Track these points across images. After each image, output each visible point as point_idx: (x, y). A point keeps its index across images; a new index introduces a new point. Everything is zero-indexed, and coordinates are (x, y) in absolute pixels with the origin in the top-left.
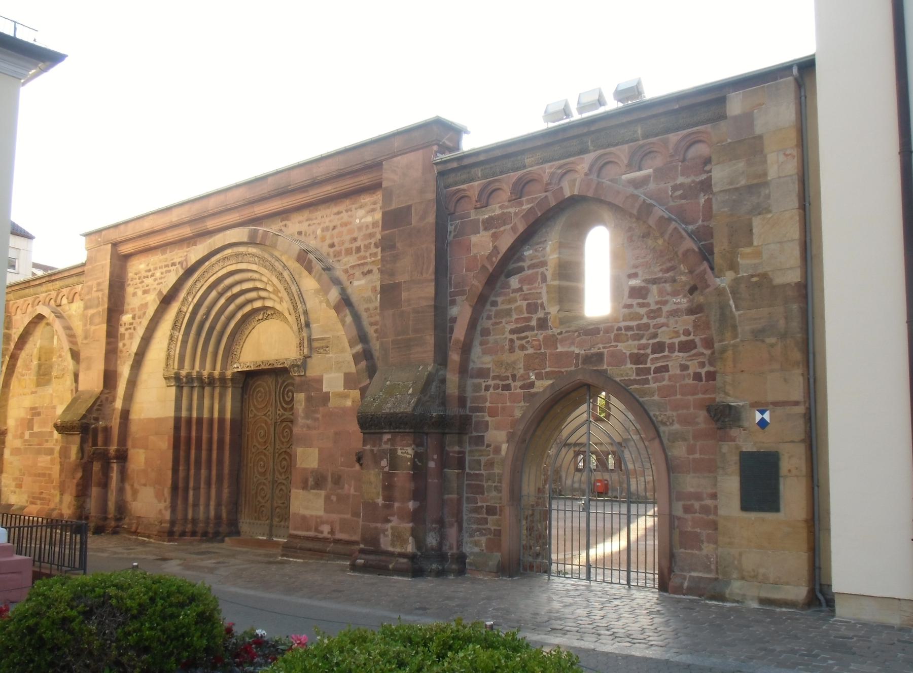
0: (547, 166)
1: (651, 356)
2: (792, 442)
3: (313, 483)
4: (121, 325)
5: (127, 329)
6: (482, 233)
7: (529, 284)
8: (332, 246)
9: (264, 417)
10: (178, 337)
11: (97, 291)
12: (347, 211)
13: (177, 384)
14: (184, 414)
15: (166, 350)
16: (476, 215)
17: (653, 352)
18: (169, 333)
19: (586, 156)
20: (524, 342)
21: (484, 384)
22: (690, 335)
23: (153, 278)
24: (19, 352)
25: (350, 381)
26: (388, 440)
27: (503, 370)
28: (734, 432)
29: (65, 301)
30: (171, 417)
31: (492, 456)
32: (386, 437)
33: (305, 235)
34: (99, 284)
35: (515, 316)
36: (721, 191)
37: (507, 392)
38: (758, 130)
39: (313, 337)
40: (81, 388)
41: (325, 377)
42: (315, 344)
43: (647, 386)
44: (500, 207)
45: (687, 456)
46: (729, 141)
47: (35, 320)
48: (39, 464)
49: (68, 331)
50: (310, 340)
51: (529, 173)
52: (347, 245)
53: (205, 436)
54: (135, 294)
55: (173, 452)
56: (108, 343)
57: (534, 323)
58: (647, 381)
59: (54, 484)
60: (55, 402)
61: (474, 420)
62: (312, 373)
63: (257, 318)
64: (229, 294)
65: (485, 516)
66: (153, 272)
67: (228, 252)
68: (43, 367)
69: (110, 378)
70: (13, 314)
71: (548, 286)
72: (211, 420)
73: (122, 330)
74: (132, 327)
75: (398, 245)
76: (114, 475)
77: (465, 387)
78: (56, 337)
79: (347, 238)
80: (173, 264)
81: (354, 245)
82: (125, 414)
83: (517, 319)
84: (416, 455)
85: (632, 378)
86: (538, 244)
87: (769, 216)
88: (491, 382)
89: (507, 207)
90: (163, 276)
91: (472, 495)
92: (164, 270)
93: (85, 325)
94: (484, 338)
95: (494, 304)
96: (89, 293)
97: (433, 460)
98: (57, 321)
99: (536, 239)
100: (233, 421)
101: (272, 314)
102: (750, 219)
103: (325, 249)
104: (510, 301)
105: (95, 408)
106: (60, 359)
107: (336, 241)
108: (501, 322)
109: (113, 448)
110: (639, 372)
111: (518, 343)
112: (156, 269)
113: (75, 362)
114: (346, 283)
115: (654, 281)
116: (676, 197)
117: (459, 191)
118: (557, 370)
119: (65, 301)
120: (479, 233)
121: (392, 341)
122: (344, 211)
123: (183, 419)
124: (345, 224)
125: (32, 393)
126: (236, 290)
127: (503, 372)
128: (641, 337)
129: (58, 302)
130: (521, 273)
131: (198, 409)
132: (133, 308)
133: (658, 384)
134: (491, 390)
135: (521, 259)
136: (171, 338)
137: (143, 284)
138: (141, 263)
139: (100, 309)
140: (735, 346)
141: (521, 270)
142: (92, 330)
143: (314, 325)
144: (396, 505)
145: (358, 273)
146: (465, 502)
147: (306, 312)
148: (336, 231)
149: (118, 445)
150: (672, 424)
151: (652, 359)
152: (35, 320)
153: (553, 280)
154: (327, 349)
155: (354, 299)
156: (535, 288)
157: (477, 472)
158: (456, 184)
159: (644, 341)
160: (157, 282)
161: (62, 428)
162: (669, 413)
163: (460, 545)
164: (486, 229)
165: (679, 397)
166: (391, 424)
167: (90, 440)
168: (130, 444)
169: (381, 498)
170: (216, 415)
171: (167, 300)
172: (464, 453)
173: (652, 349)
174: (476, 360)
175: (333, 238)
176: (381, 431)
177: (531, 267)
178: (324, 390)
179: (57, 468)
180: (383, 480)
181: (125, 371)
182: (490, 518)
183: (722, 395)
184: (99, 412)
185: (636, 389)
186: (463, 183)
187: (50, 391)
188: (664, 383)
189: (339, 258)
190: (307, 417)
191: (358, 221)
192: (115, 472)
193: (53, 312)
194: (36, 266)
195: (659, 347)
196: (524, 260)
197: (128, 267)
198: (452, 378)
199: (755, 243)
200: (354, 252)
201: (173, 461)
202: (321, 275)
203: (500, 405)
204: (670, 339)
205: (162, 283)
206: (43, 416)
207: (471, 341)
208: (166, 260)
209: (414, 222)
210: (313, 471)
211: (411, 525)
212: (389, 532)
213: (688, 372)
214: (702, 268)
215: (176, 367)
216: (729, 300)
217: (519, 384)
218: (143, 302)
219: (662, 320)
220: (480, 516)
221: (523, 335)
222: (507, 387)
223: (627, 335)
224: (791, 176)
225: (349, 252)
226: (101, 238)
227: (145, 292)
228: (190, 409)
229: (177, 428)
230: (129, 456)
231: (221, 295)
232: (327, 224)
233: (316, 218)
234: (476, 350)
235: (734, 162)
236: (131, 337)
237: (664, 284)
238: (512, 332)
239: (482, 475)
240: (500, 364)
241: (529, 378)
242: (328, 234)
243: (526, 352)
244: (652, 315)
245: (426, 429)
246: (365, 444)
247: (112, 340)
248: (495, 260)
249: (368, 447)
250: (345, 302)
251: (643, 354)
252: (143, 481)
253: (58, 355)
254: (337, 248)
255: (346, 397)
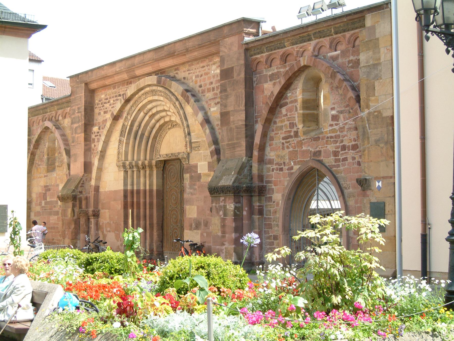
0: (295, 46)
1: (341, 152)
2: (389, 197)
3: (195, 226)
4: (92, 133)
5: (96, 136)
6: (269, 83)
7: (290, 112)
8: (200, 86)
9: (174, 188)
10: (123, 140)
11: (78, 112)
12: (207, 66)
13: (124, 170)
14: (129, 188)
15: (117, 148)
16: (266, 72)
17: (342, 150)
18: (118, 138)
19: (311, 42)
20: (288, 144)
21: (271, 168)
22: (356, 141)
23: (109, 104)
24: (36, 150)
25: (210, 167)
26: (223, 200)
27: (280, 160)
28: (368, 192)
29: (60, 118)
30: (122, 190)
31: (275, 207)
32: (222, 199)
33: (187, 80)
34: (79, 108)
35: (284, 130)
36: (363, 66)
37: (281, 172)
38: (377, 36)
39: (192, 141)
40: (72, 173)
41: (199, 164)
42: (193, 145)
43: (339, 168)
44: (277, 68)
45: (355, 205)
46: (366, 40)
47: (44, 130)
48: (51, 222)
49: (63, 137)
50: (191, 143)
51: (288, 50)
52: (208, 86)
53: (142, 200)
54: (99, 114)
55: (124, 211)
56: (85, 145)
57: (292, 134)
58: (338, 166)
59: (60, 233)
60: (58, 182)
61: (267, 188)
62: (192, 162)
63: (168, 127)
64: (150, 113)
65: (273, 241)
66: (109, 100)
67: (148, 89)
68: (50, 160)
69: (87, 167)
70: (31, 126)
71: (298, 113)
72: (145, 191)
73: (93, 136)
74: (99, 134)
75: (228, 89)
76: (92, 226)
77: (262, 170)
78: (56, 140)
79: (208, 82)
80: (120, 95)
81: (212, 86)
82: (97, 189)
83: (285, 131)
84: (236, 208)
85: (333, 164)
86: (294, 90)
87: (381, 81)
88: (275, 167)
89: (280, 68)
90: (114, 102)
91: (267, 230)
92: (115, 99)
93: (72, 134)
94: (271, 142)
95: (275, 123)
96: (74, 114)
97: (245, 210)
98: (57, 131)
99: (293, 87)
100: (157, 191)
101: (176, 125)
102: (374, 82)
103: (197, 88)
104: (282, 122)
105: (80, 185)
106: (60, 155)
107: (202, 83)
108: (278, 133)
109: (91, 209)
110: (336, 161)
111: (286, 145)
112: (110, 98)
113: (68, 157)
114: (207, 109)
115: (341, 112)
116: (349, 67)
117: (257, 58)
118: (302, 160)
119: (60, 118)
120: (267, 82)
121: (227, 144)
122: (206, 66)
123: (128, 191)
124: (206, 74)
125: (45, 176)
126: (154, 111)
127: (279, 160)
128: (336, 142)
129: (57, 118)
130: (286, 105)
131: (137, 184)
132: (99, 122)
133: (343, 167)
134: (275, 171)
135: (286, 98)
136: (120, 141)
137: (104, 107)
138: (102, 95)
139: (80, 124)
140: (368, 148)
141: (286, 104)
142: (76, 137)
143: (193, 134)
144: (227, 235)
145: (213, 104)
146: (263, 234)
147: (188, 126)
148: (202, 77)
149: (94, 208)
150: (349, 188)
151: (341, 154)
152: (44, 130)
153: (300, 110)
154: (199, 148)
155: (211, 119)
156: (292, 114)
157: (269, 217)
158: (255, 54)
159: (338, 144)
160: (111, 106)
161: (62, 199)
162: (348, 183)
163: (261, 257)
164: (270, 80)
165: (352, 174)
166: (223, 192)
167: (78, 205)
168: (100, 207)
169: (220, 232)
170: (148, 188)
171: (116, 118)
172: (263, 206)
173: (341, 149)
174: (267, 154)
175: (201, 82)
176: (219, 195)
177: (292, 102)
178: (199, 172)
179: (60, 223)
180: (221, 223)
181: (96, 162)
182: (275, 242)
183: (364, 173)
184: (82, 188)
185: (335, 170)
186: (259, 54)
187: (55, 175)
188: (346, 167)
189: (204, 94)
190: (191, 188)
191: (213, 72)
192: (93, 224)
193: (54, 125)
194: (45, 79)
195: (344, 148)
196: (287, 99)
197: (95, 96)
198: (255, 166)
199: (376, 95)
200: (211, 90)
201: (124, 217)
202: (193, 105)
203: (278, 179)
204: (348, 143)
205: (114, 107)
206: (51, 191)
207: (265, 144)
208: (116, 92)
209: (235, 77)
210: (195, 219)
211: (233, 246)
212: (224, 251)
213: (355, 161)
214: (356, 107)
215: (123, 159)
216: (366, 124)
217: (287, 167)
218: (105, 119)
219: (345, 133)
220: (271, 241)
221: (288, 140)
222: (281, 169)
223: (331, 141)
224: (389, 60)
225: (209, 90)
226: (78, 79)
227: (105, 112)
228: (132, 185)
229: (125, 196)
230: (100, 215)
231: (146, 114)
232: (198, 73)
233: (192, 70)
234: (268, 149)
235: (368, 51)
236: (98, 141)
237: (345, 114)
238: (284, 138)
239: (271, 218)
240: (278, 156)
241: (291, 164)
242: (198, 79)
243: (289, 150)
244: (341, 130)
245: (241, 194)
246: (212, 203)
247: (88, 143)
248: (273, 99)
249: (214, 204)
250: (207, 121)
251: (337, 151)
252: (108, 229)
253: (58, 152)
254: (203, 88)
255: (209, 175)
